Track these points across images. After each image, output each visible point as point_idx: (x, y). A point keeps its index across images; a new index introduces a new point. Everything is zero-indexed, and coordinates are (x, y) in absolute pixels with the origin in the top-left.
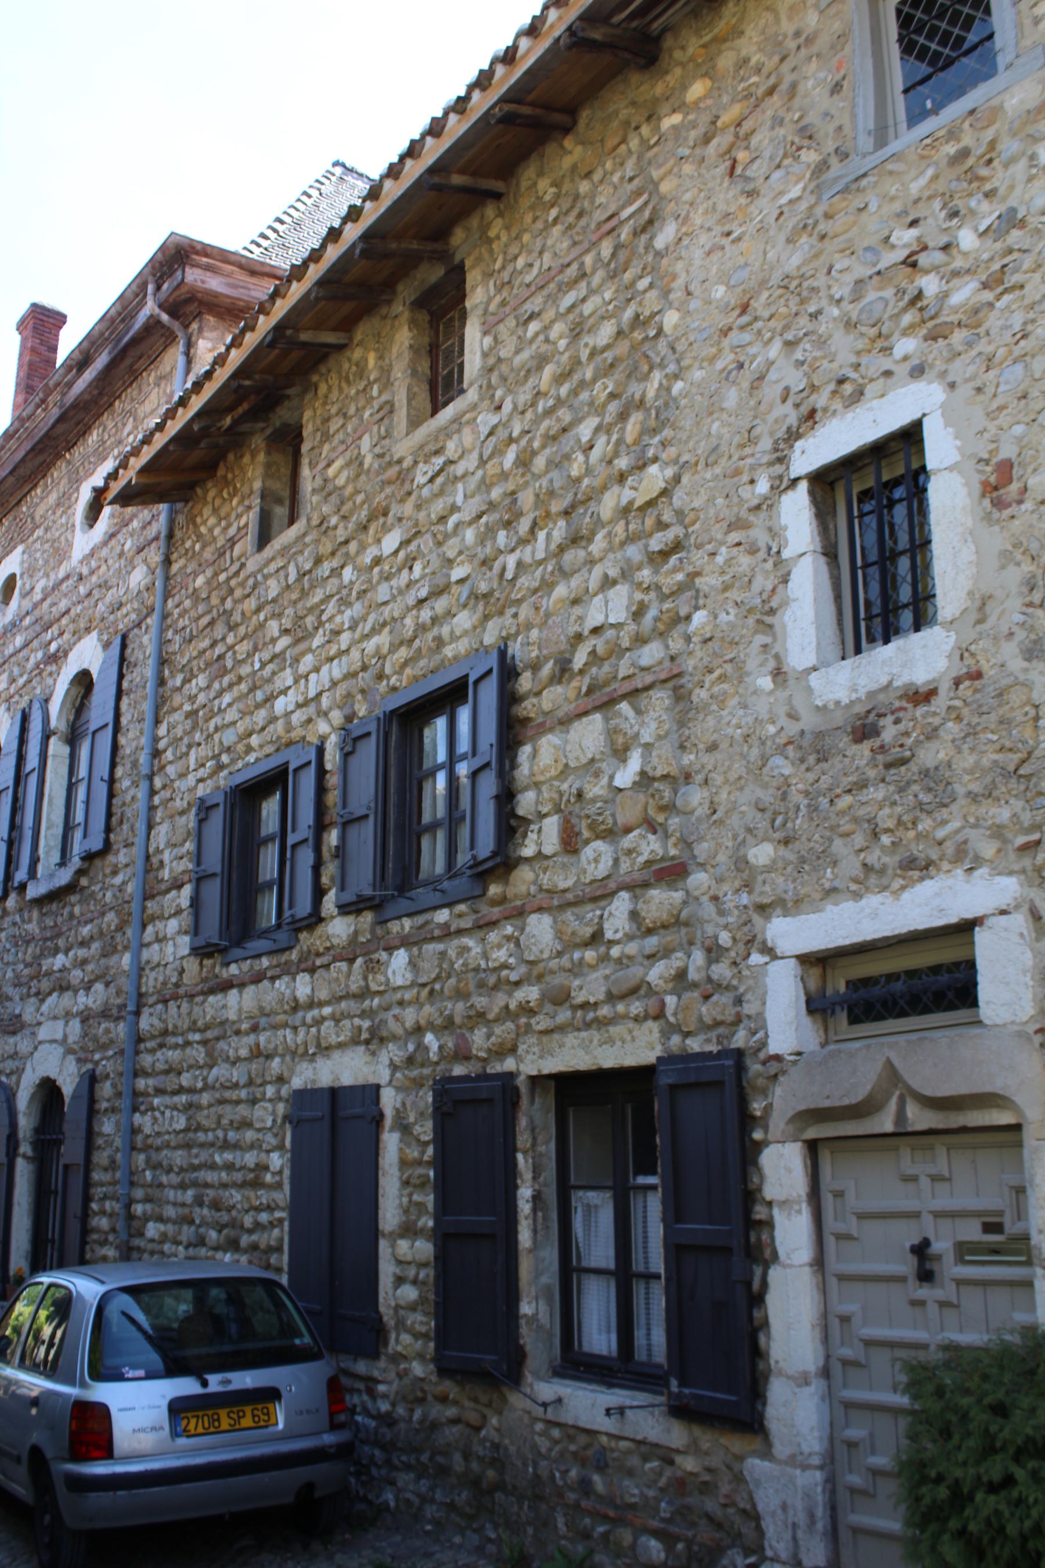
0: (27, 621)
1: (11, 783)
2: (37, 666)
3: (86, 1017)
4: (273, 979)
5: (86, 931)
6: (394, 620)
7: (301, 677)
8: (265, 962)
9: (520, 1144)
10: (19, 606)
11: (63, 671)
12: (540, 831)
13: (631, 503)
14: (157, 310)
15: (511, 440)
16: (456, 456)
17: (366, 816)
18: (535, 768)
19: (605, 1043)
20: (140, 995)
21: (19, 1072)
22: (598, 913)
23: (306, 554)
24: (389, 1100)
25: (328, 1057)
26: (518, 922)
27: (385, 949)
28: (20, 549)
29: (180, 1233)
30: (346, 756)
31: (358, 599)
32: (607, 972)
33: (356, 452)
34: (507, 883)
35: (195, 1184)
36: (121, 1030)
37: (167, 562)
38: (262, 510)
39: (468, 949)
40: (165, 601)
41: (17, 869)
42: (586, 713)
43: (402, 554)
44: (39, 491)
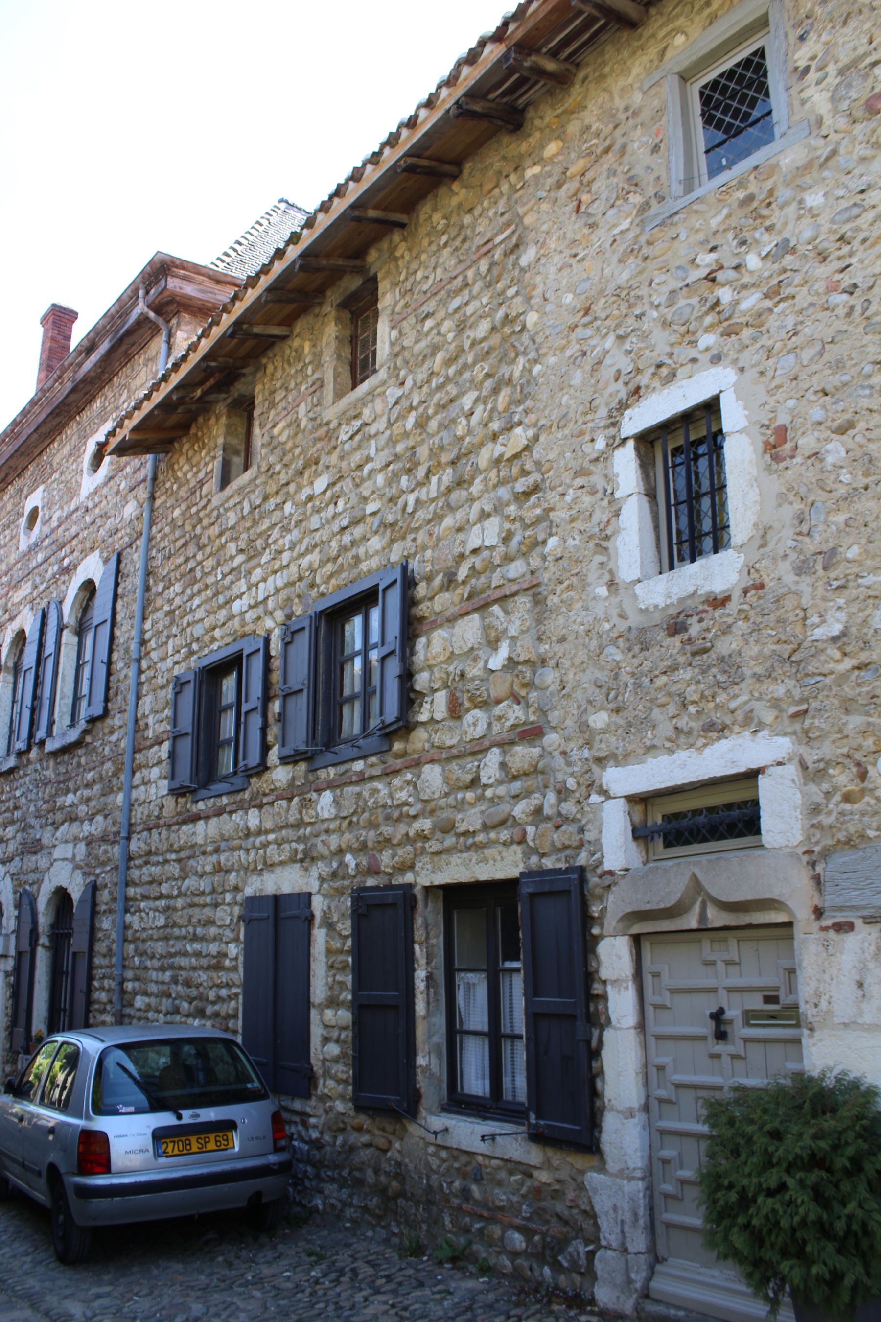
0: (47, 542)
1: (33, 664)
3: (89, 841)
5: (89, 776)
7: (252, 585)
8: (225, 800)
9: (416, 938)
13: (502, 455)
15: (411, 408)
17: (301, 691)
19: (481, 861)
20: (131, 825)
21: (39, 882)
22: (476, 764)
24: (318, 904)
26: (416, 771)
27: (315, 791)
28: (41, 488)
34: (407, 741)
35: (172, 967)
37: (152, 498)
38: (224, 459)
40: (151, 528)
42: (467, 614)
44: (56, 444)
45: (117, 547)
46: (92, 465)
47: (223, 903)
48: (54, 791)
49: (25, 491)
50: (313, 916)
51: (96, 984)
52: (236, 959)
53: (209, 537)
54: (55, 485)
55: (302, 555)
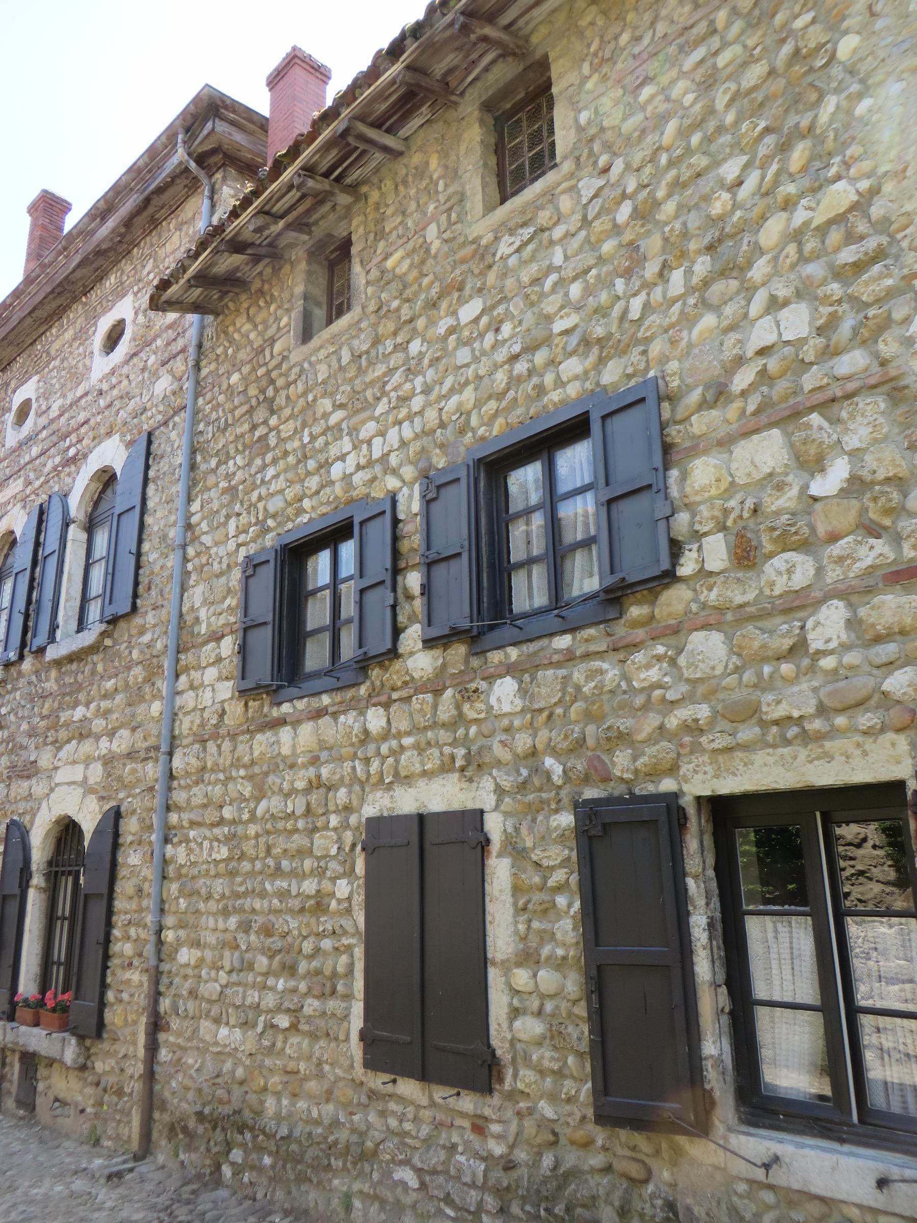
0: (44, 434)
1: (28, 565)
2: (55, 469)
3: (108, 761)
4: (335, 715)
5: (110, 684)
6: (479, 378)
7: (362, 442)
8: (326, 700)
9: (688, 868)
10: (35, 424)
11: (82, 471)
12: (700, 549)
13: (807, 223)
14: (186, 157)
15: (624, 196)
16: (551, 223)
17: (459, 555)
18: (688, 490)
19: (818, 758)
20: (173, 737)
21: (34, 813)
22: (798, 624)
23: (362, 337)
24: (494, 825)
25: (410, 785)
26: (672, 641)
27: (483, 679)
28: (35, 378)
29: (221, 958)
30: (428, 503)
31: (430, 366)
32: (815, 684)
33: (421, 240)
34: (653, 603)
35: (240, 910)
36: (152, 771)
37: (197, 367)
38: (305, 308)
39: (602, 672)
40: (196, 399)
41: (34, 636)
42: (756, 431)
43: (484, 320)
44: (54, 331)
45: (145, 427)
46: (104, 346)
47: (326, 827)
48: (56, 705)
49: (13, 385)
50: (488, 841)
51: (116, 933)
52: (349, 899)
53: (288, 397)
54: (54, 373)
55: (446, 397)
